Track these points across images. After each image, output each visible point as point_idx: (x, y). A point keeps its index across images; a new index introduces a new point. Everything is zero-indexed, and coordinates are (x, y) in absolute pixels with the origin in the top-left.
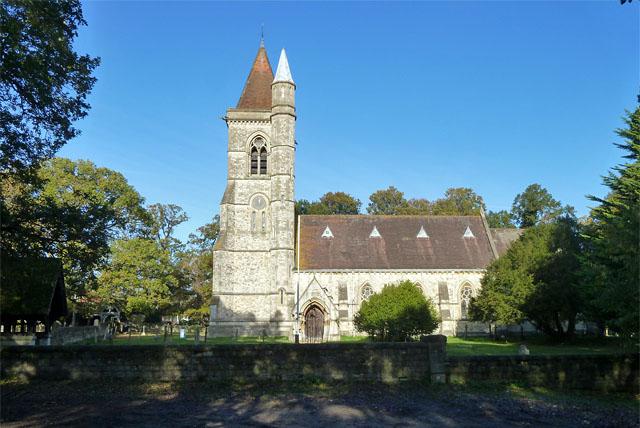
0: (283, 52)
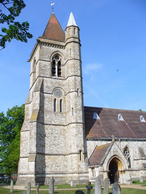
0: (71, 15)
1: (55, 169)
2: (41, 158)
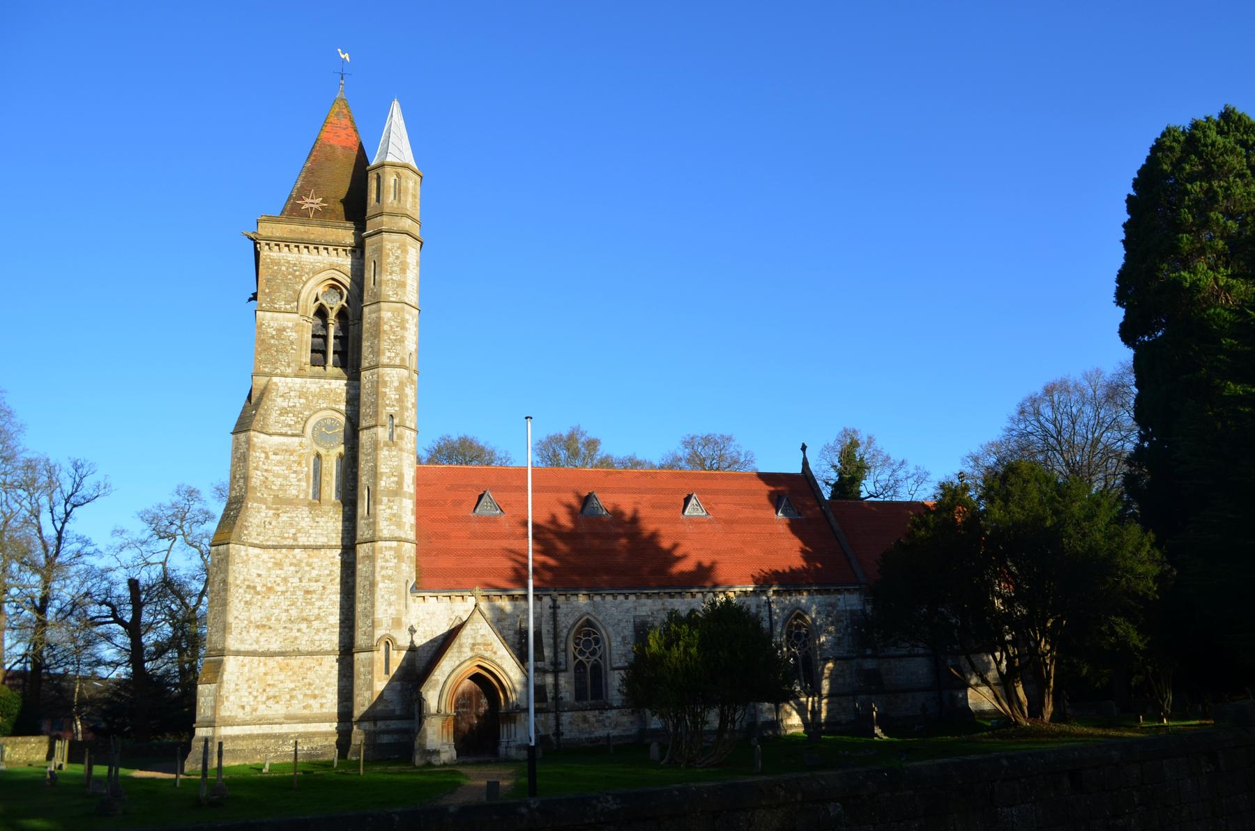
0: (396, 109)
1: (304, 708)
2: (250, 671)
